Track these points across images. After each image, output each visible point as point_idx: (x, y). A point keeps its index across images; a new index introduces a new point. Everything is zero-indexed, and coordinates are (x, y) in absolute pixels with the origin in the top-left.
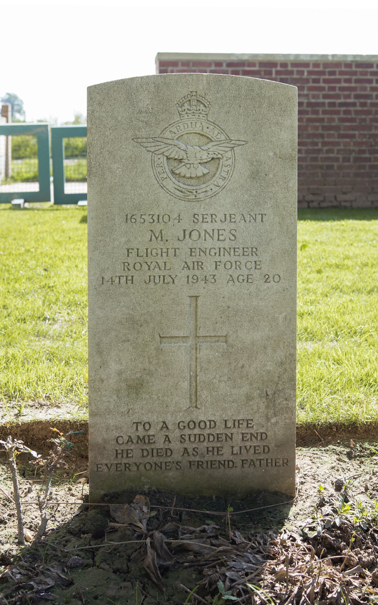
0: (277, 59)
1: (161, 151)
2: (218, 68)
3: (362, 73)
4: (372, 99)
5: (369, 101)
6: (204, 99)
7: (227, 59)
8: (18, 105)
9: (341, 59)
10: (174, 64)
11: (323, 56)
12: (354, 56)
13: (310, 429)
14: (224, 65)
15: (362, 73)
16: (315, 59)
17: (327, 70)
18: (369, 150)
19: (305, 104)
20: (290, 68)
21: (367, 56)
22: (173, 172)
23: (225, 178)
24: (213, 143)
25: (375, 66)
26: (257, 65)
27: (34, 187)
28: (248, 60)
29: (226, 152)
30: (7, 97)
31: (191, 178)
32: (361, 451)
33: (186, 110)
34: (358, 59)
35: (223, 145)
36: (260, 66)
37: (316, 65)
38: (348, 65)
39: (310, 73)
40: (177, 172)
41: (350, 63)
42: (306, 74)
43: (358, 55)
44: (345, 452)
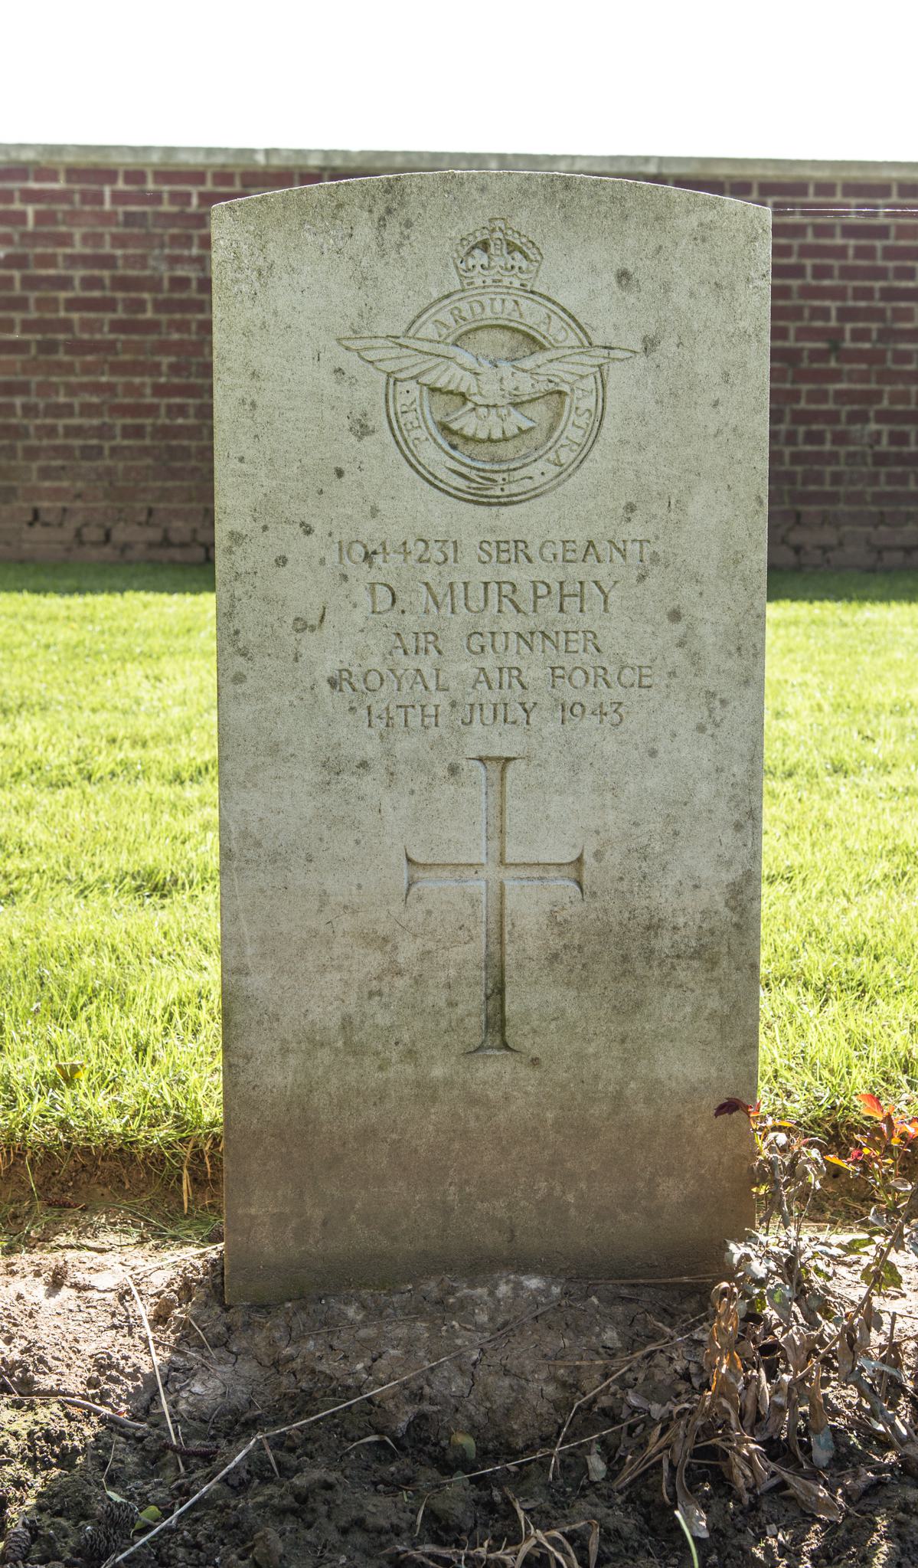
0: (115, 159)
1: (415, 371)
9: (291, 163)
11: (241, 152)
12: (327, 154)
16: (219, 160)
19: (194, 284)
20: (150, 186)
21: (362, 153)
22: (444, 428)
24: (549, 355)
28: (36, 163)
36: (69, 180)
37: (135, 176)
39: (118, 198)
40: (455, 426)
42: (195, 201)
43: (335, 151)
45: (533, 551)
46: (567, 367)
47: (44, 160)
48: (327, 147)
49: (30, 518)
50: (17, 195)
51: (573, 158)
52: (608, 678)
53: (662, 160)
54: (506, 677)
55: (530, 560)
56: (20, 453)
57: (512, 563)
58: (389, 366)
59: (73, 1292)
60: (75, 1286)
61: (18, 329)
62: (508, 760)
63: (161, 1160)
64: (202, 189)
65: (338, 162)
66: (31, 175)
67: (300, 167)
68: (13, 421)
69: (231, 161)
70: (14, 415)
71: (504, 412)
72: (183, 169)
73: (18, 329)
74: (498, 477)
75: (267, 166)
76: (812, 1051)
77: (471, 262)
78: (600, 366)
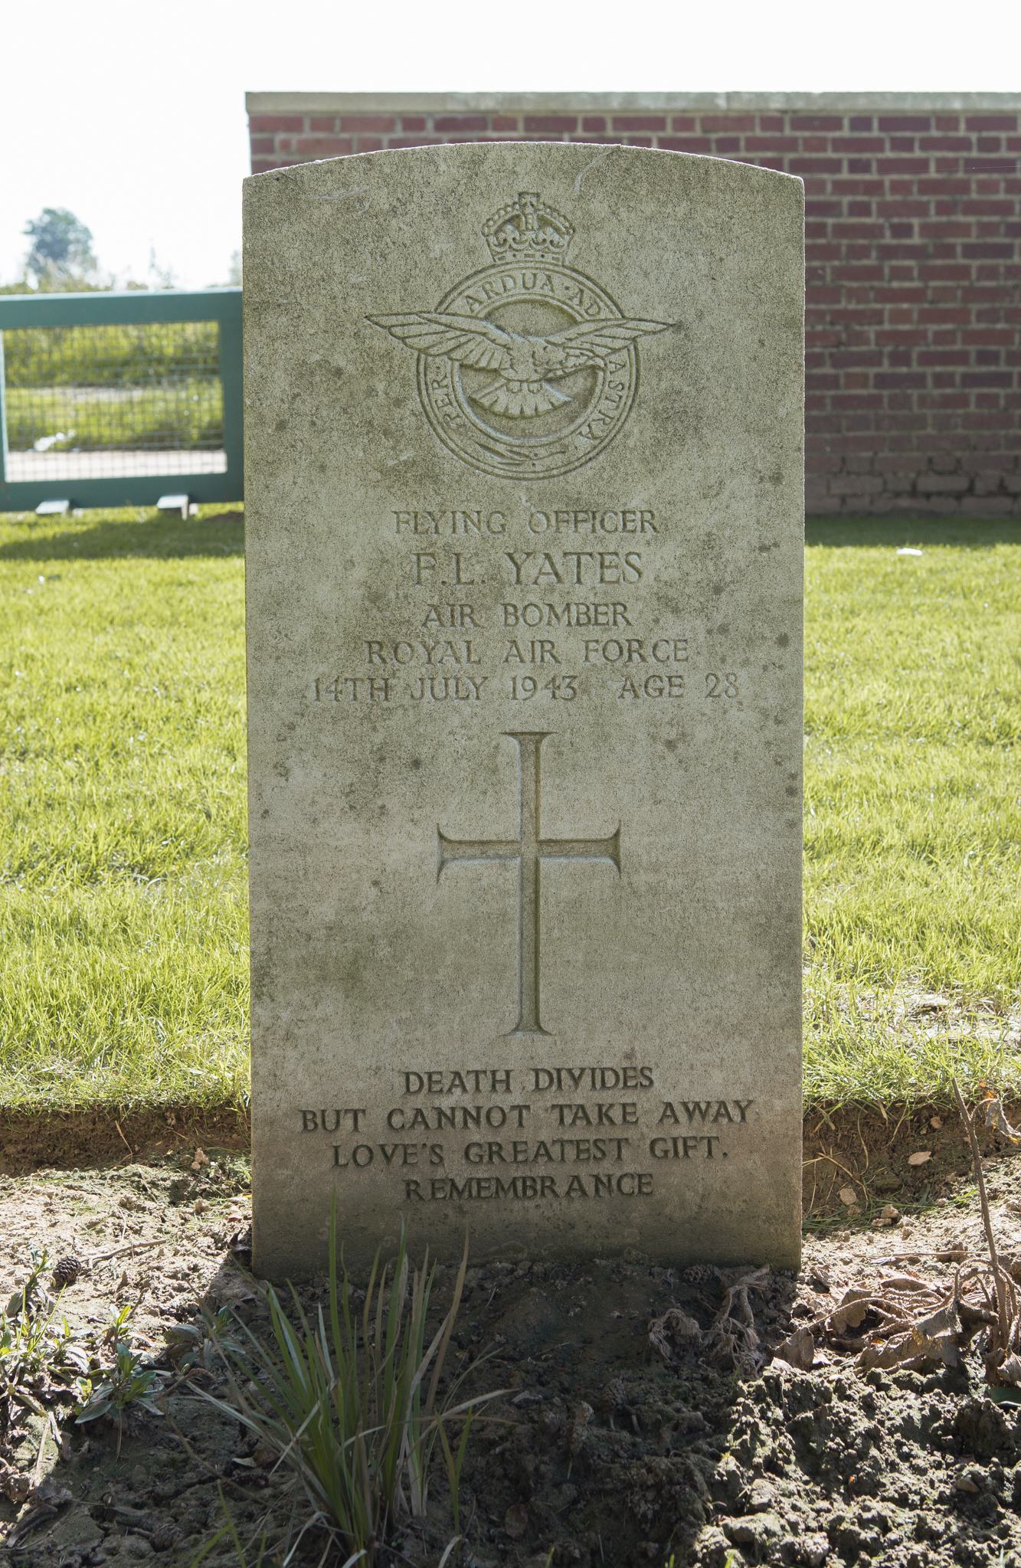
0: (575, 106)
3: (810, 145)
4: (840, 215)
5: (830, 221)
7: (436, 107)
8: (78, 241)
9: (753, 107)
10: (292, 123)
12: (788, 96)
13: (103, 1119)
14: (430, 125)
15: (810, 145)
16: (680, 105)
17: (714, 136)
18: (831, 355)
21: (824, 95)
25: (846, 123)
26: (521, 125)
27: (214, 463)
28: (496, 112)
29: (615, 351)
30: (47, 219)
32: (215, 1180)
34: (800, 105)
35: (604, 332)
38: (772, 122)
41: (778, 115)
43: (798, 94)
44: (168, 1183)
46: (598, 340)
48: (788, 90)
57: (638, 533)
58: (422, 343)
62: (543, 734)
64: (662, 134)
66: (490, 125)
67: (761, 111)
75: (728, 110)
76: (883, 1022)
78: (634, 339)
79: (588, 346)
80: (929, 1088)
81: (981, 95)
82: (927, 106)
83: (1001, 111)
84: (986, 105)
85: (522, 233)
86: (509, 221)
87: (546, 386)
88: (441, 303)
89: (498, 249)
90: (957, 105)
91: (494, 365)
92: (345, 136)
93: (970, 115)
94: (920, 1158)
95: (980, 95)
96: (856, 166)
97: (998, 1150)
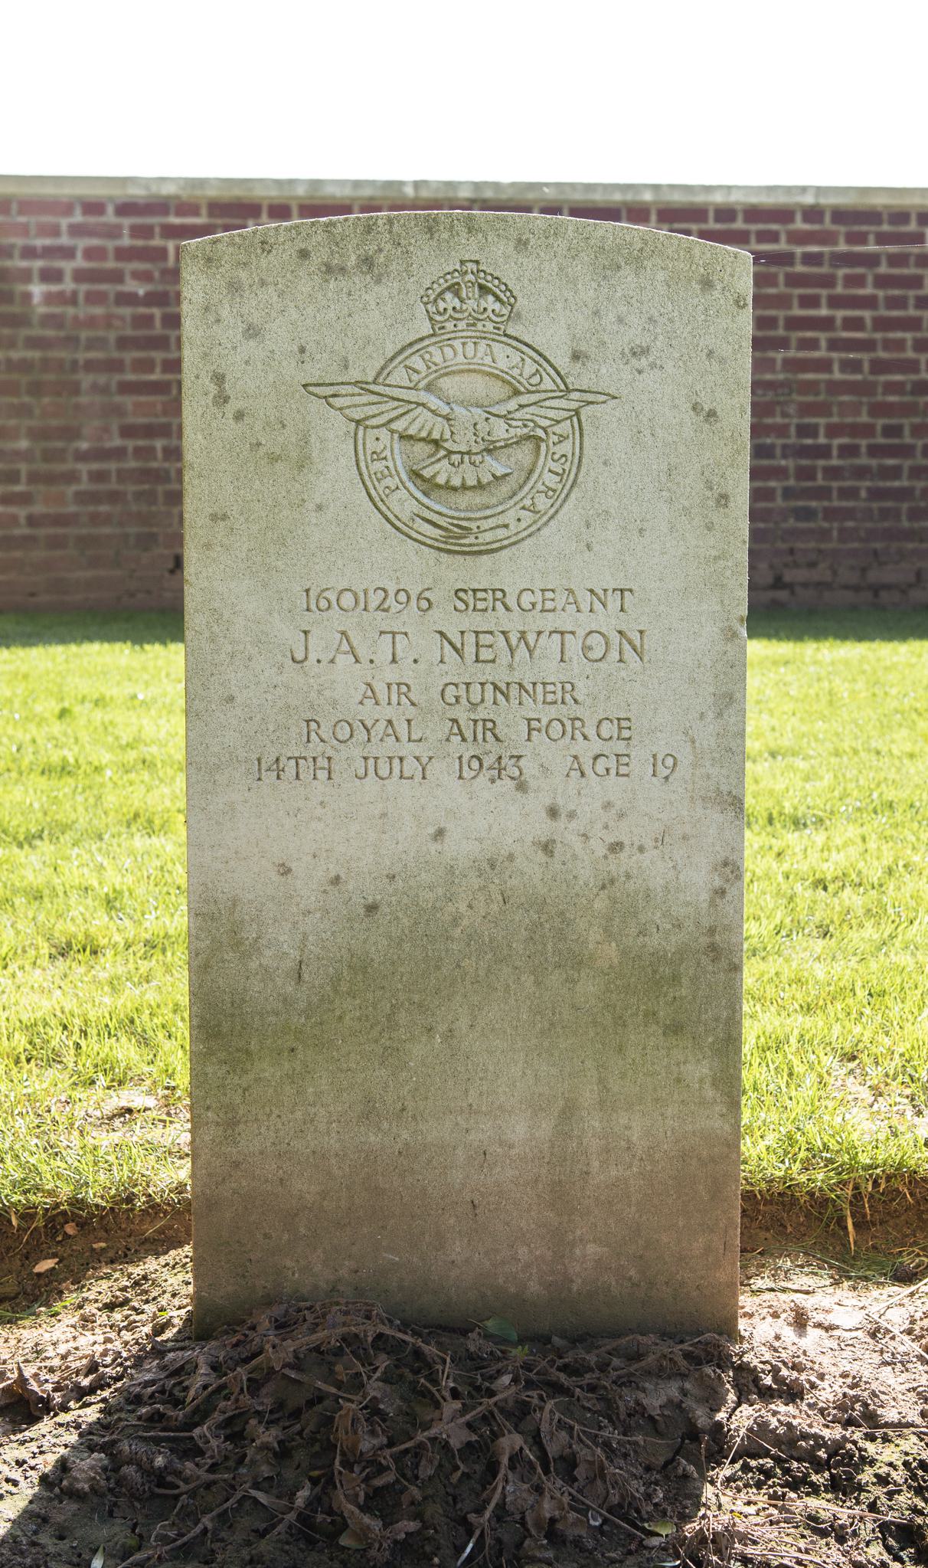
0: (259, 192)
2: (92, 220)
6: (496, 282)
7: (117, 192)
11: (389, 184)
14: (110, 209)
21: (513, 184)
22: (415, 475)
23: (554, 491)
26: (204, 211)
28: (177, 197)
31: (464, 487)
33: (450, 311)
35: (547, 403)
36: (211, 214)
45: (511, 601)
46: (543, 412)
47: (185, 194)
49: (171, 565)
50: (157, 230)
51: (729, 188)
52: (585, 730)
53: (819, 190)
54: (480, 729)
55: (507, 609)
56: (161, 499)
58: (357, 414)
59: (819, 1332)
60: (819, 1325)
61: (158, 369)
63: (825, 1202)
65: (489, 194)
68: (155, 465)
69: (378, 193)
70: (155, 459)
71: (478, 459)
72: (330, 202)
73: (158, 369)
74: (473, 525)
76: (812, 1101)
77: (442, 305)
79: (528, 417)
80: (65, 1191)
81: (672, 187)
82: (618, 197)
83: (692, 204)
84: (678, 198)
85: (462, 301)
86: (448, 288)
87: (488, 458)
88: (379, 374)
89: (438, 318)
90: (648, 197)
91: (436, 435)
92: (22, 219)
93: (661, 206)
94: (45, 1265)
95: (672, 187)
96: (851, 238)
97: (126, 1256)
